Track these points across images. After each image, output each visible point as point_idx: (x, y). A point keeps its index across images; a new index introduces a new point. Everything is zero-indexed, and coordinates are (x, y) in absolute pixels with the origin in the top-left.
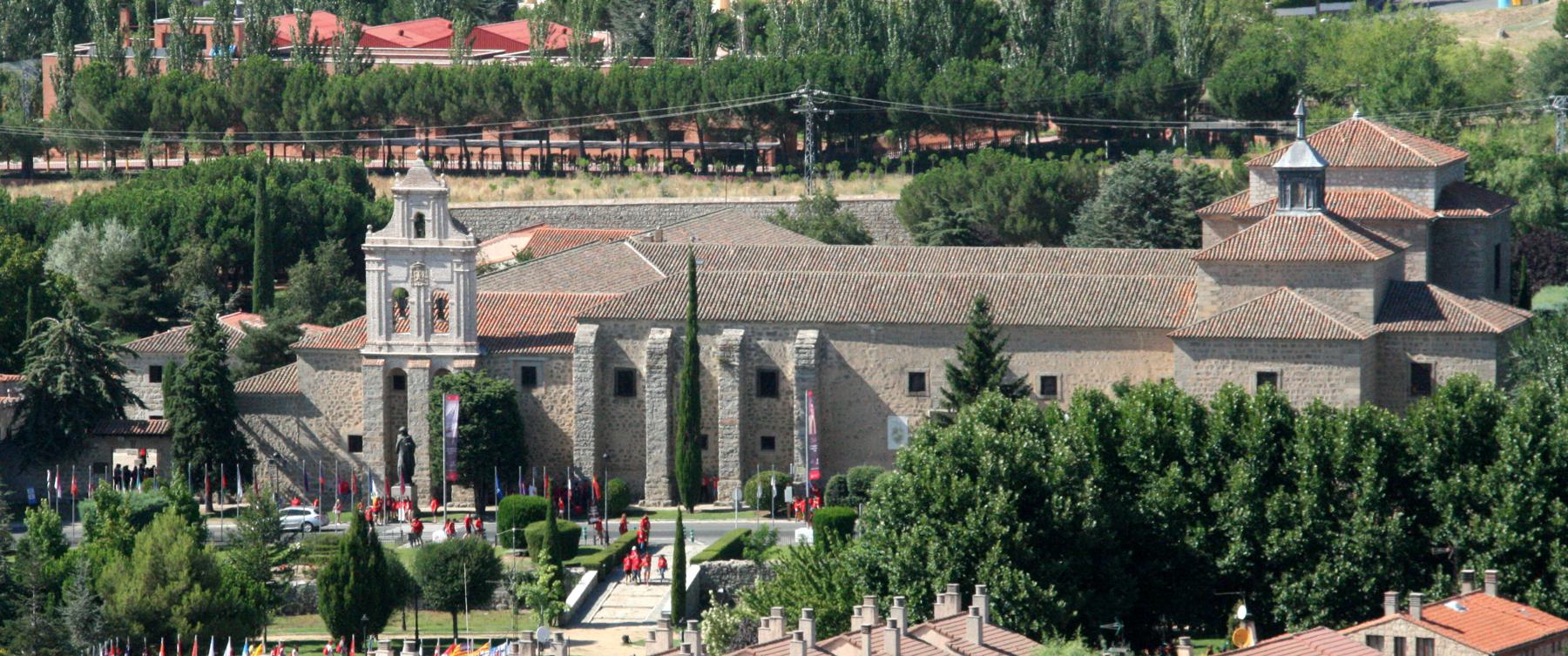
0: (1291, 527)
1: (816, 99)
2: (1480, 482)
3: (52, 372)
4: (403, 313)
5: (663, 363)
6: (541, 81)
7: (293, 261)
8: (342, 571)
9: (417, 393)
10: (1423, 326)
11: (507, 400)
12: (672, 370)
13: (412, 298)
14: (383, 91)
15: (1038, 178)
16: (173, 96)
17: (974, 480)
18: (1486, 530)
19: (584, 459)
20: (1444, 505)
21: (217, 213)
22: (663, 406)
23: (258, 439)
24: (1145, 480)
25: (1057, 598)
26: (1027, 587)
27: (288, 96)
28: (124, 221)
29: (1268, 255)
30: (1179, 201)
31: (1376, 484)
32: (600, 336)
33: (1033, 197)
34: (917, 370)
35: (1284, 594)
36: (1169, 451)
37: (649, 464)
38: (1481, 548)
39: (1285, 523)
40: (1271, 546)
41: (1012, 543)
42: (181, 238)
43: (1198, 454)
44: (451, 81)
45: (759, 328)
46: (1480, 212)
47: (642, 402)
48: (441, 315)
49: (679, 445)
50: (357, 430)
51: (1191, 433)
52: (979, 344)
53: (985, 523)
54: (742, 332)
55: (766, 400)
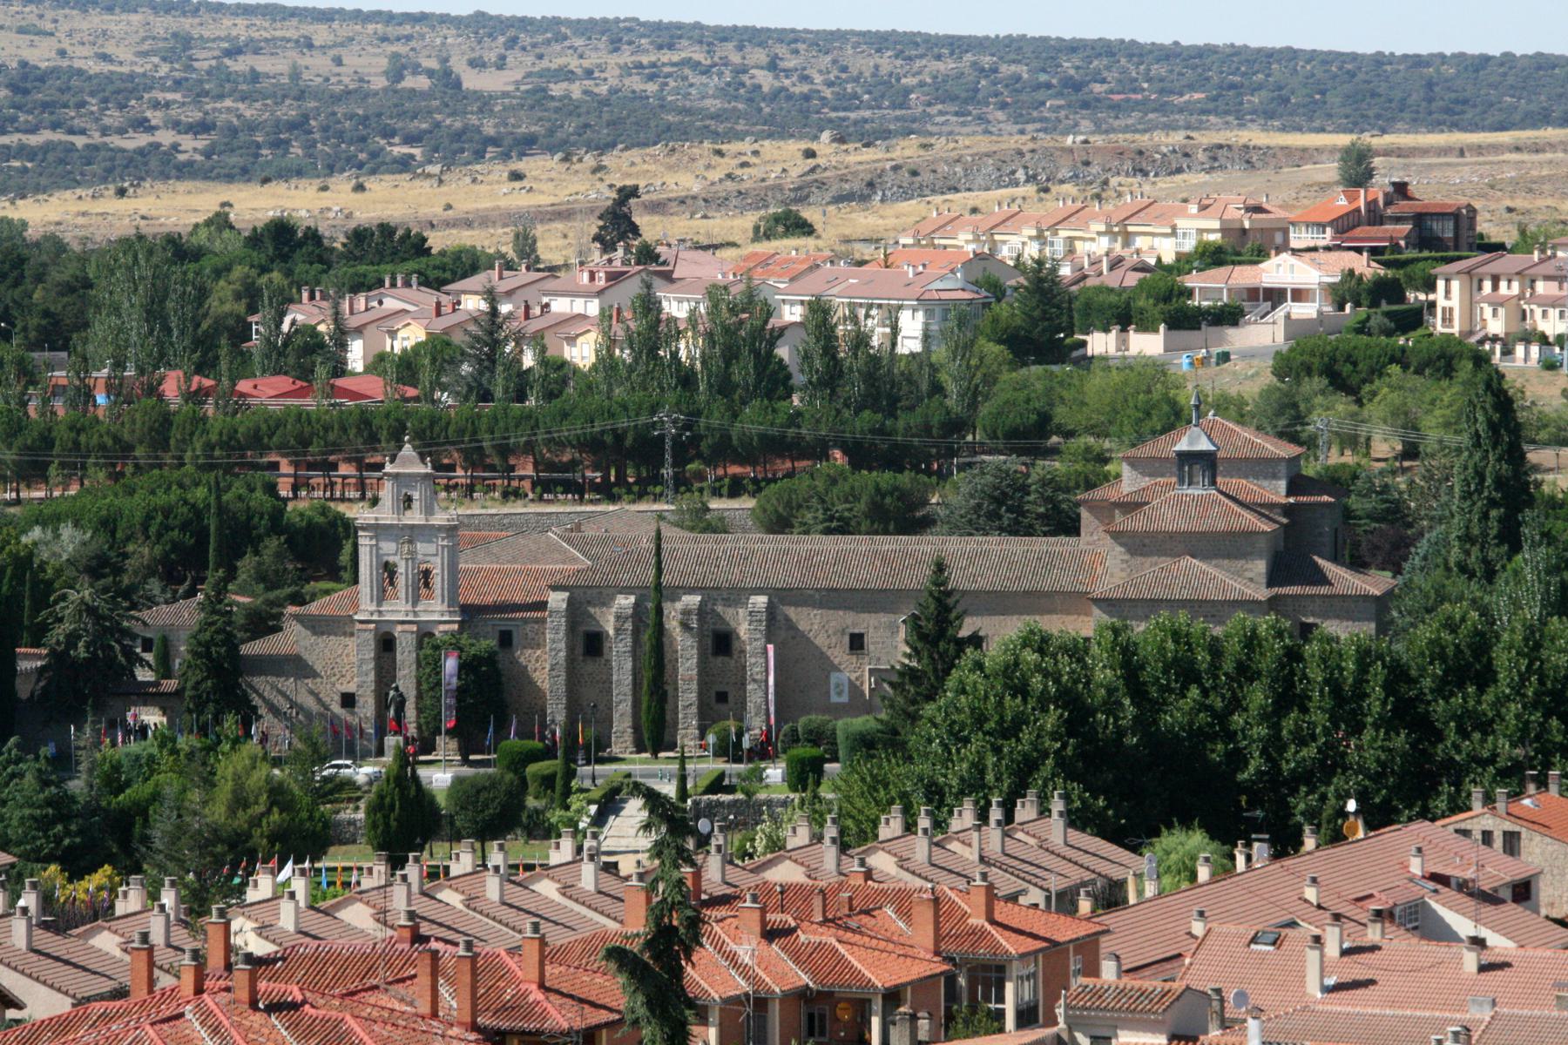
0: (1306, 745)
1: (675, 422)
2: (1479, 702)
3: (72, 639)
4: (392, 583)
5: (629, 626)
6: (397, 420)
7: (241, 555)
8: (388, 800)
9: (406, 655)
10: (1309, 590)
11: (490, 659)
12: (636, 633)
13: (401, 569)
14: (258, 429)
15: (878, 489)
16: (73, 435)
17: (1025, 701)
18: (1489, 745)
19: (557, 713)
20: (1446, 723)
21: (160, 518)
22: (629, 665)
23: (264, 699)
24: (1165, 703)
25: (1106, 808)
26: (1080, 798)
27: (175, 435)
28: (76, 524)
29: (1171, 527)
30: (1031, 498)
31: (1384, 703)
32: (570, 602)
33: (874, 503)
34: (856, 631)
35: (1302, 806)
36: (1187, 673)
37: (616, 716)
38: (1484, 763)
39: (1302, 740)
40: (1288, 762)
41: (1063, 758)
42: (128, 539)
43: (1216, 677)
44: (318, 421)
45: (715, 594)
46: (1326, 498)
47: (608, 661)
48: (427, 585)
49: (645, 699)
50: (351, 688)
51: (1208, 658)
52: (938, 600)
53: (1038, 736)
54: (699, 598)
55: (720, 659)
